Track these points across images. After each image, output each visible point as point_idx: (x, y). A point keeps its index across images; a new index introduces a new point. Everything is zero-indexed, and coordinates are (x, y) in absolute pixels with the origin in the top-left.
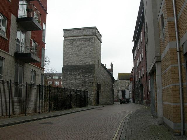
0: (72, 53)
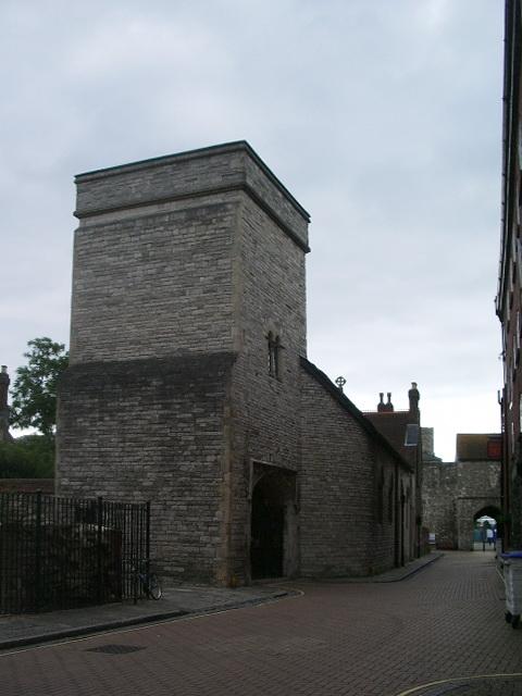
0: (116, 293)
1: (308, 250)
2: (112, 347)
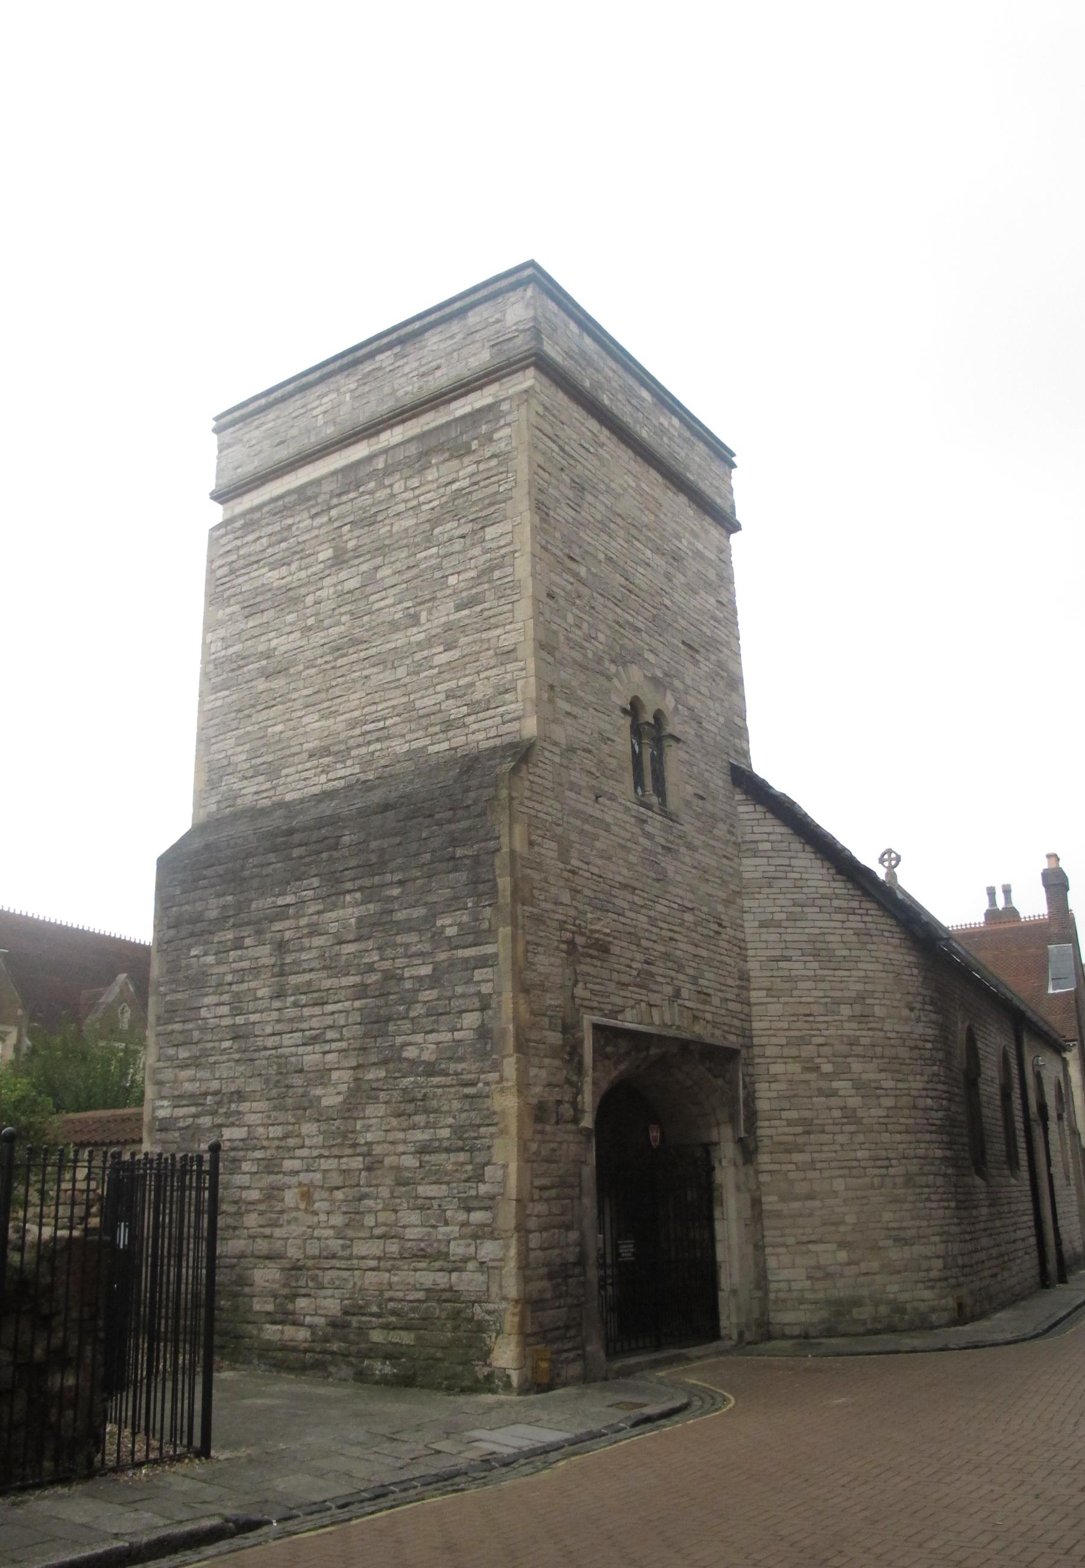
0: (282, 644)
1: (736, 527)
2: (272, 771)
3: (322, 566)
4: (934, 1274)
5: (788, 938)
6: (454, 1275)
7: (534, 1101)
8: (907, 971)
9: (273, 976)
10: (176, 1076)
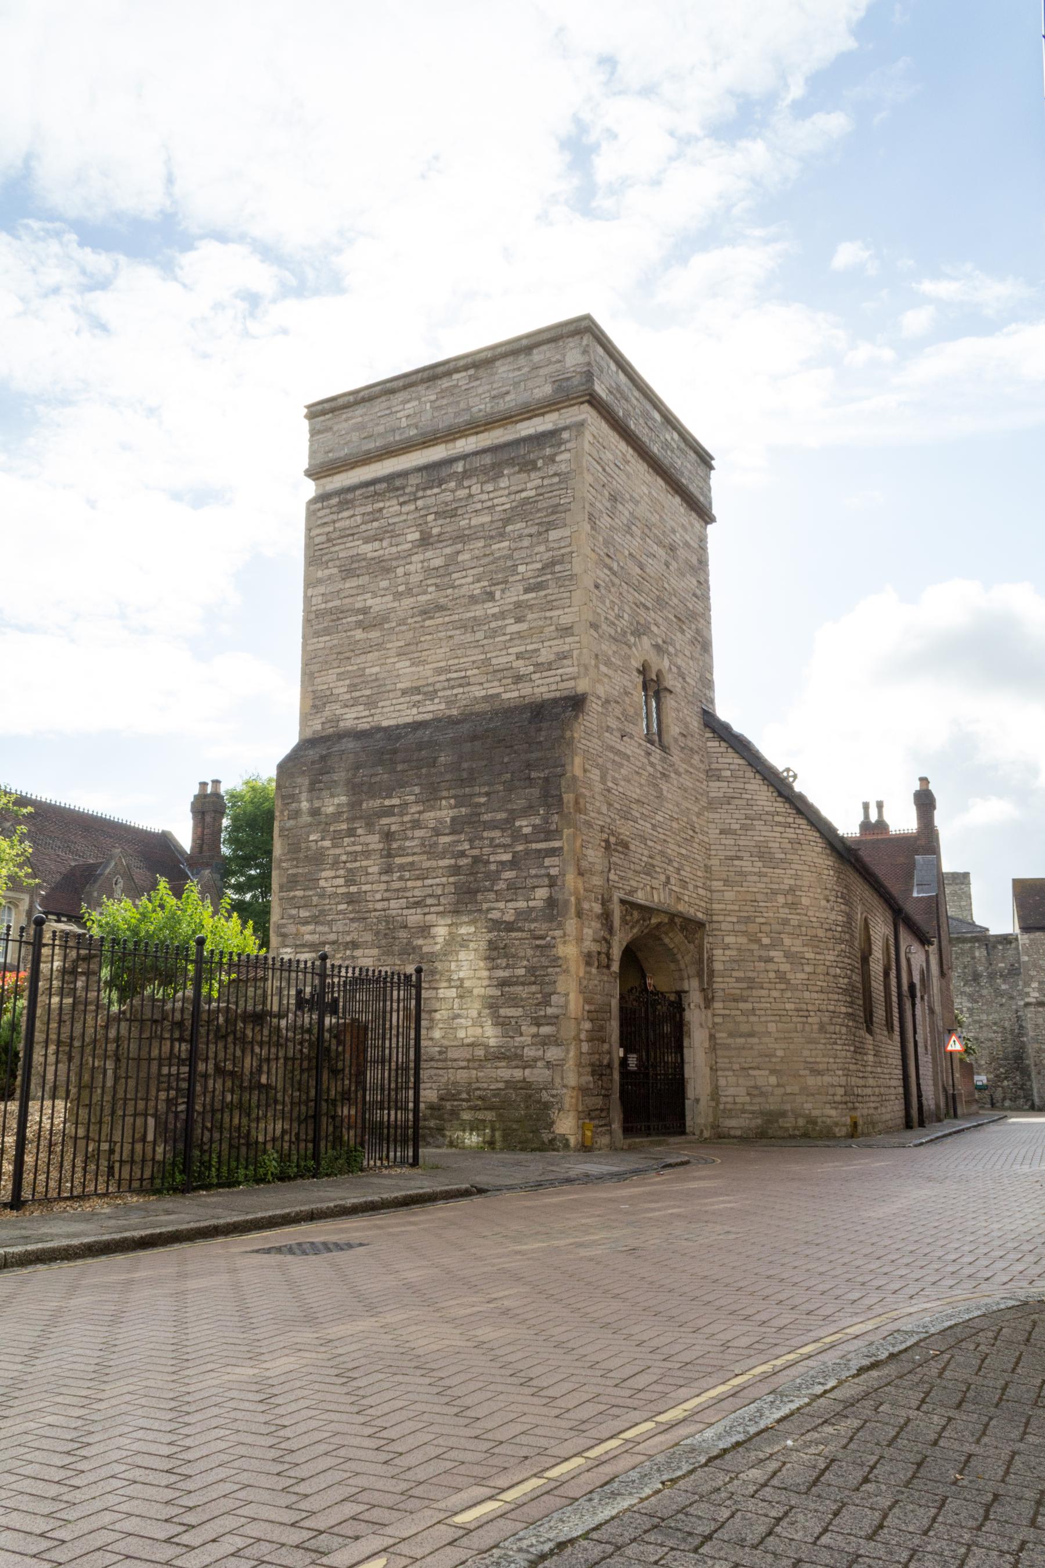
0: (376, 604)
2: (371, 703)
3: (410, 545)
4: (838, 1098)
5: (741, 843)
6: (527, 1071)
7: (586, 951)
8: (826, 872)
9: (382, 857)
10: (297, 930)
